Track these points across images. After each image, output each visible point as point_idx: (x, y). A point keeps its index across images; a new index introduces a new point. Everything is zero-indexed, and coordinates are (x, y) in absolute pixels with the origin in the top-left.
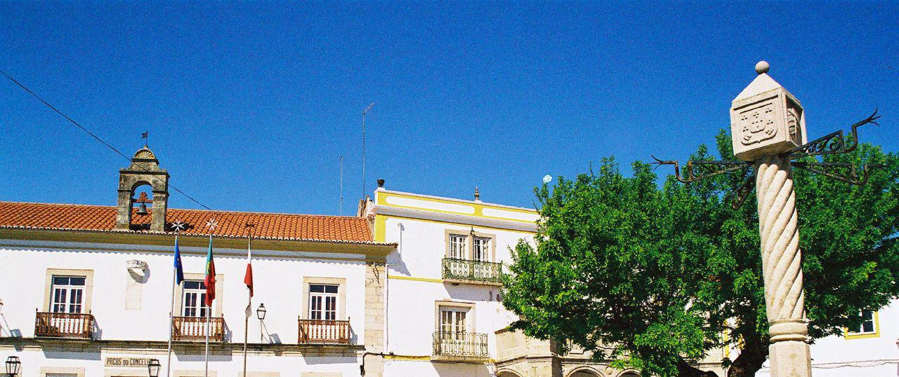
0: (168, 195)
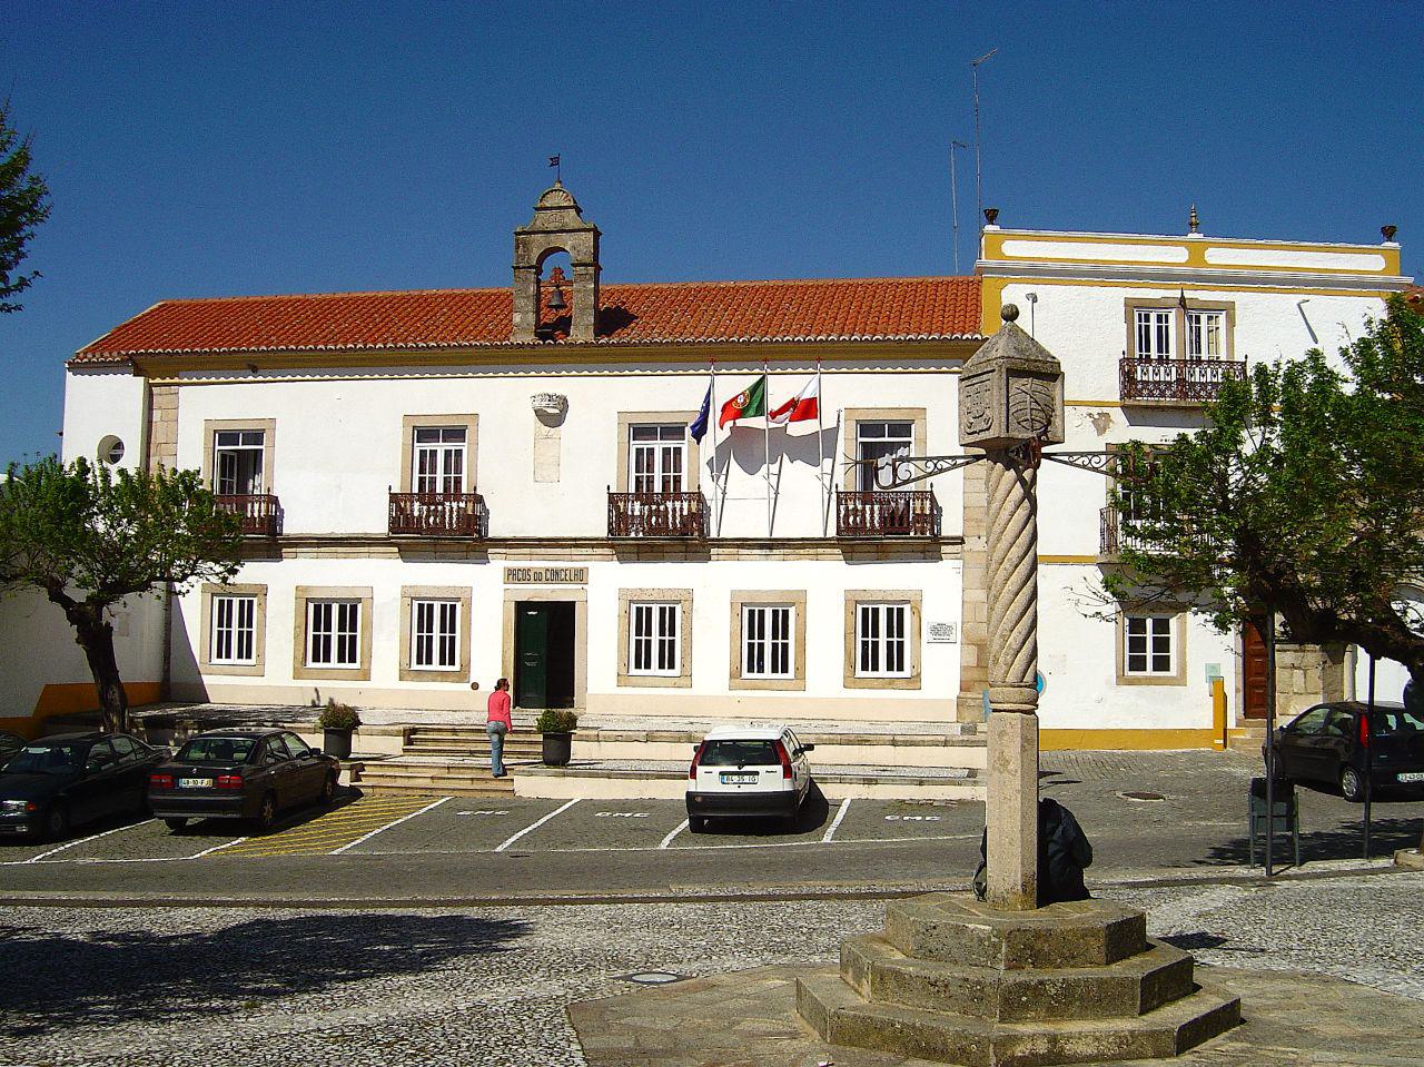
0: (598, 269)
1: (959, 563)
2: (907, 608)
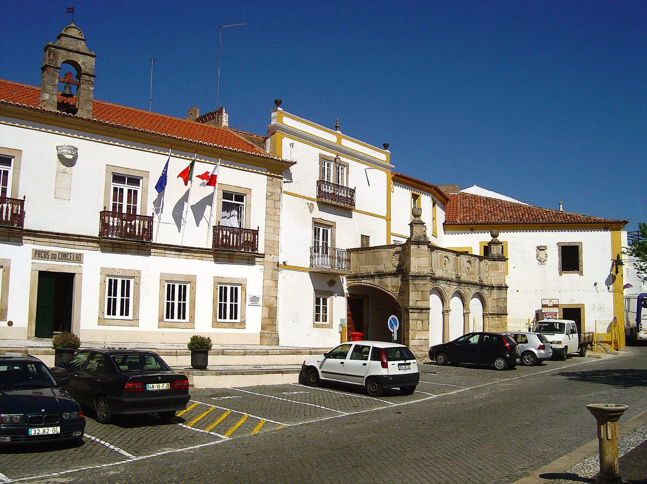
1: (262, 267)
2: (239, 288)
